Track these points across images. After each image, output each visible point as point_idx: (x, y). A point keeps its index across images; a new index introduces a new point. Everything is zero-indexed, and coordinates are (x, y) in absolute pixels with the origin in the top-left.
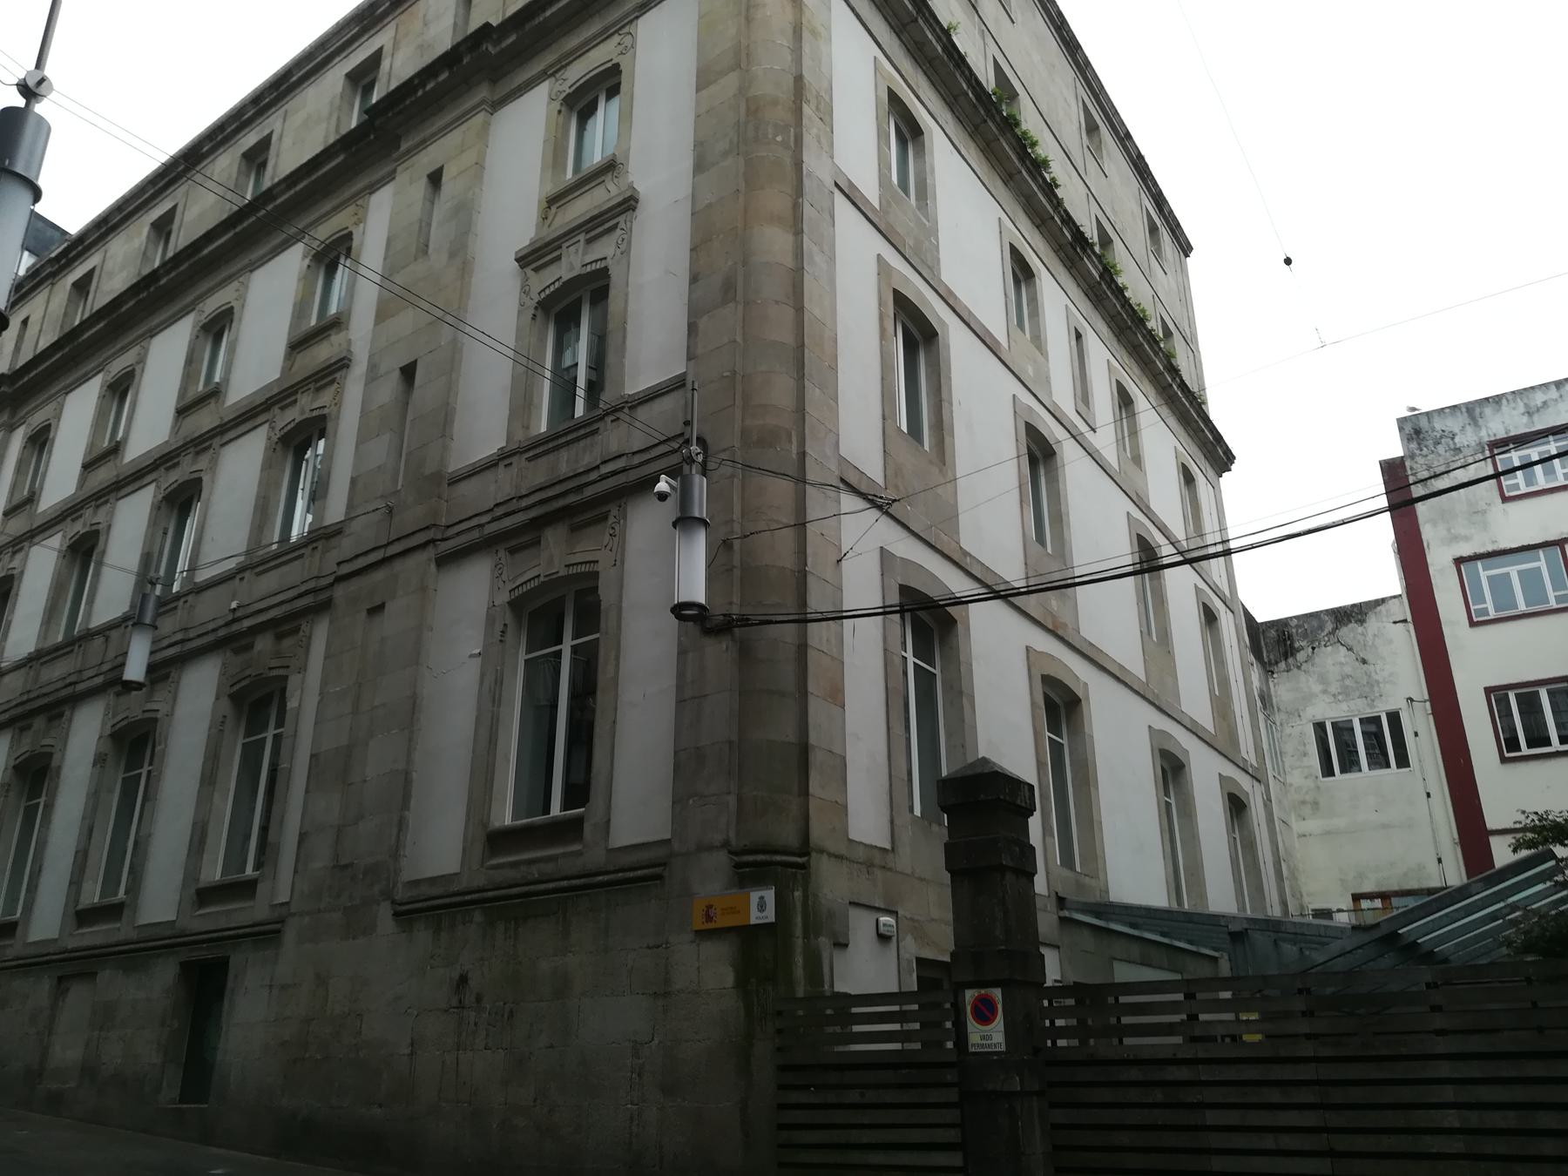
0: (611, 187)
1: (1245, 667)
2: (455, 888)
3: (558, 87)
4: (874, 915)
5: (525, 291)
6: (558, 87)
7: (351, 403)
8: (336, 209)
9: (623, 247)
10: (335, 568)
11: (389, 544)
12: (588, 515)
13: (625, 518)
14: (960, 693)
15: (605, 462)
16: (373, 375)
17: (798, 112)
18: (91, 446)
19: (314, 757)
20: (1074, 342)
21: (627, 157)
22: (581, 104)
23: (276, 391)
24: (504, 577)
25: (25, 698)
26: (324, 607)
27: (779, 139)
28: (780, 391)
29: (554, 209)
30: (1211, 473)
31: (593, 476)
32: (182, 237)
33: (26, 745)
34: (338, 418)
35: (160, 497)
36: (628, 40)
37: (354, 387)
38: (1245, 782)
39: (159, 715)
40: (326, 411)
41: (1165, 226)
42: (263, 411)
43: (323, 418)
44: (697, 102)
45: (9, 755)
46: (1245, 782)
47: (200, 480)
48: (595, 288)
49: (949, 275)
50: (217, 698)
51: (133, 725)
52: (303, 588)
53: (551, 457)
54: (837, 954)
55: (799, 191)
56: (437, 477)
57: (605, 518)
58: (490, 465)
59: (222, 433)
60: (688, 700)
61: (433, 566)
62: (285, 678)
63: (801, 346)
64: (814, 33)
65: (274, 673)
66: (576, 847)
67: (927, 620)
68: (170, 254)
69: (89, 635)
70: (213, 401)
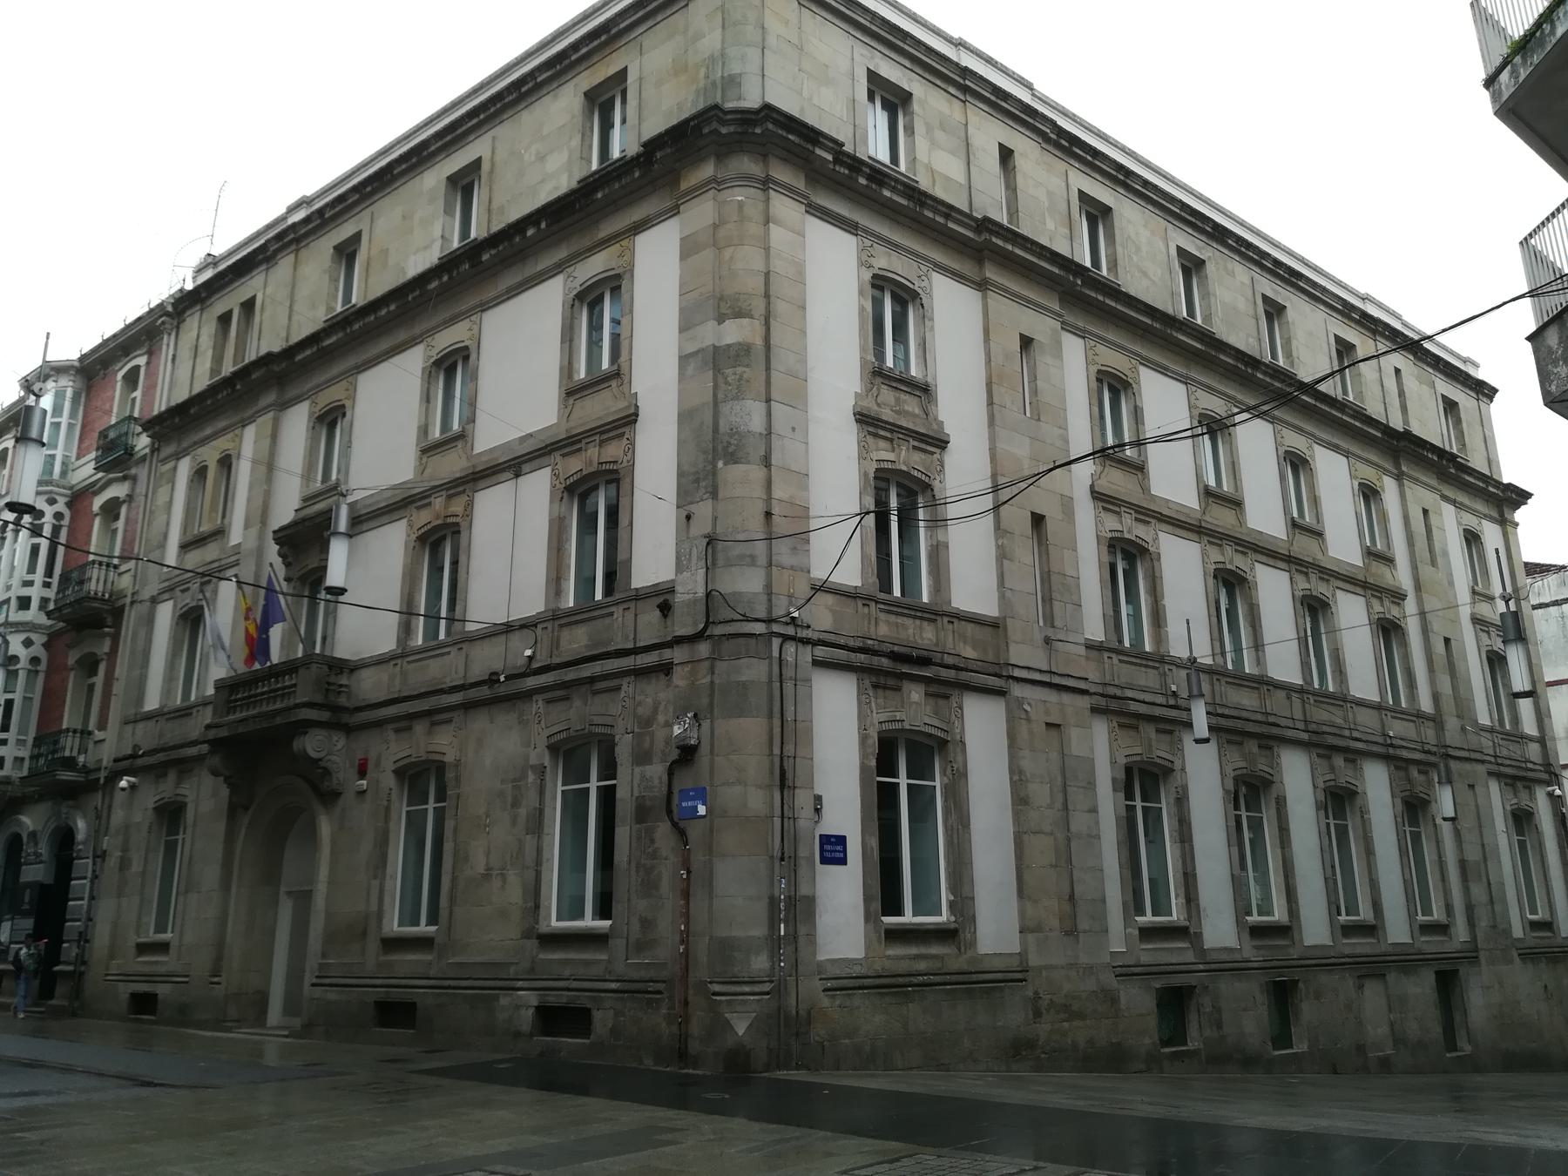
6: (569, 284)
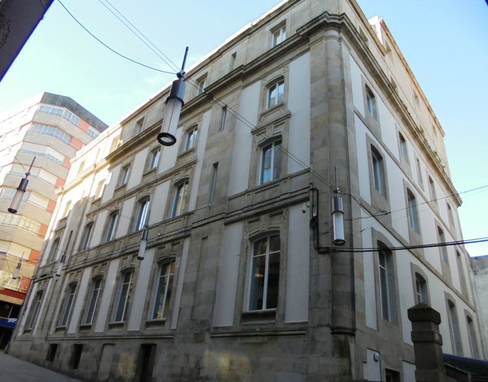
0: (283, 112)
1: (469, 272)
2: (230, 331)
3: (264, 82)
4: (374, 352)
5: (254, 141)
7: (197, 175)
8: (193, 117)
9: (287, 129)
10: (191, 224)
11: (209, 218)
12: (275, 212)
13: (289, 213)
14: (393, 277)
15: (281, 195)
16: (204, 166)
17: (344, 90)
18: (117, 185)
19: (184, 284)
20: (417, 162)
21: (287, 102)
22: (271, 86)
23: (173, 170)
24: (247, 230)
25: (96, 258)
26: (189, 236)
27: (338, 97)
28: (341, 174)
29: (263, 117)
30: (455, 206)
31: (278, 199)
32: (146, 126)
33: (96, 272)
34: (192, 178)
35: (137, 200)
36: (286, 69)
37: (198, 169)
38: (471, 312)
39: (136, 267)
40: (189, 176)
41: (437, 126)
42: (169, 176)
43: (188, 178)
44: (311, 87)
45: (91, 275)
46: (471, 312)
47: (149, 196)
48: (277, 140)
49: (384, 140)
50: (153, 263)
51: (127, 269)
52: (181, 230)
53: (263, 193)
54: (364, 364)
55: (345, 113)
56: (224, 198)
57: (281, 213)
58: (242, 195)
59: (157, 182)
60: (314, 276)
61: (223, 226)
62: (175, 258)
63: (348, 160)
64: (346, 67)
65: (172, 256)
66: (273, 321)
67: (385, 252)
68: (142, 131)
69: (115, 241)
70: (154, 173)
